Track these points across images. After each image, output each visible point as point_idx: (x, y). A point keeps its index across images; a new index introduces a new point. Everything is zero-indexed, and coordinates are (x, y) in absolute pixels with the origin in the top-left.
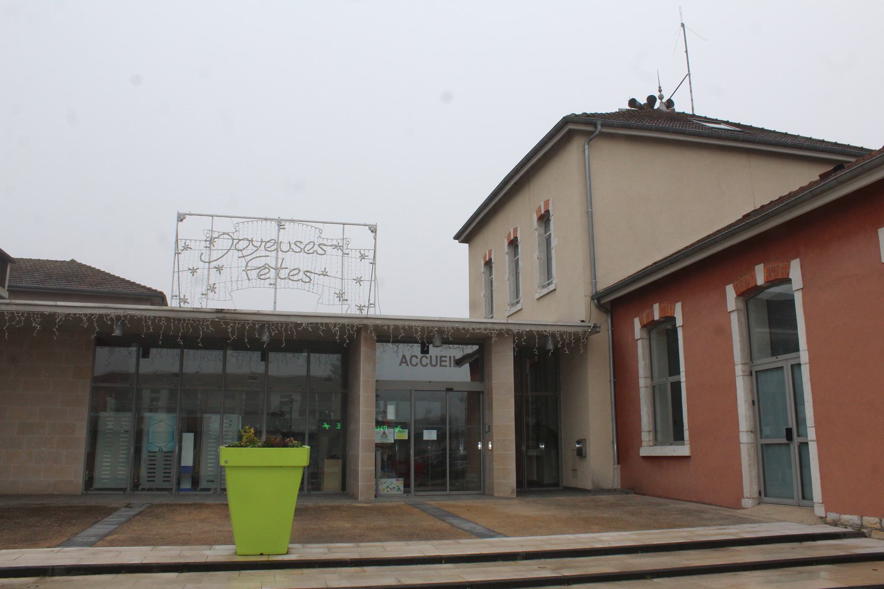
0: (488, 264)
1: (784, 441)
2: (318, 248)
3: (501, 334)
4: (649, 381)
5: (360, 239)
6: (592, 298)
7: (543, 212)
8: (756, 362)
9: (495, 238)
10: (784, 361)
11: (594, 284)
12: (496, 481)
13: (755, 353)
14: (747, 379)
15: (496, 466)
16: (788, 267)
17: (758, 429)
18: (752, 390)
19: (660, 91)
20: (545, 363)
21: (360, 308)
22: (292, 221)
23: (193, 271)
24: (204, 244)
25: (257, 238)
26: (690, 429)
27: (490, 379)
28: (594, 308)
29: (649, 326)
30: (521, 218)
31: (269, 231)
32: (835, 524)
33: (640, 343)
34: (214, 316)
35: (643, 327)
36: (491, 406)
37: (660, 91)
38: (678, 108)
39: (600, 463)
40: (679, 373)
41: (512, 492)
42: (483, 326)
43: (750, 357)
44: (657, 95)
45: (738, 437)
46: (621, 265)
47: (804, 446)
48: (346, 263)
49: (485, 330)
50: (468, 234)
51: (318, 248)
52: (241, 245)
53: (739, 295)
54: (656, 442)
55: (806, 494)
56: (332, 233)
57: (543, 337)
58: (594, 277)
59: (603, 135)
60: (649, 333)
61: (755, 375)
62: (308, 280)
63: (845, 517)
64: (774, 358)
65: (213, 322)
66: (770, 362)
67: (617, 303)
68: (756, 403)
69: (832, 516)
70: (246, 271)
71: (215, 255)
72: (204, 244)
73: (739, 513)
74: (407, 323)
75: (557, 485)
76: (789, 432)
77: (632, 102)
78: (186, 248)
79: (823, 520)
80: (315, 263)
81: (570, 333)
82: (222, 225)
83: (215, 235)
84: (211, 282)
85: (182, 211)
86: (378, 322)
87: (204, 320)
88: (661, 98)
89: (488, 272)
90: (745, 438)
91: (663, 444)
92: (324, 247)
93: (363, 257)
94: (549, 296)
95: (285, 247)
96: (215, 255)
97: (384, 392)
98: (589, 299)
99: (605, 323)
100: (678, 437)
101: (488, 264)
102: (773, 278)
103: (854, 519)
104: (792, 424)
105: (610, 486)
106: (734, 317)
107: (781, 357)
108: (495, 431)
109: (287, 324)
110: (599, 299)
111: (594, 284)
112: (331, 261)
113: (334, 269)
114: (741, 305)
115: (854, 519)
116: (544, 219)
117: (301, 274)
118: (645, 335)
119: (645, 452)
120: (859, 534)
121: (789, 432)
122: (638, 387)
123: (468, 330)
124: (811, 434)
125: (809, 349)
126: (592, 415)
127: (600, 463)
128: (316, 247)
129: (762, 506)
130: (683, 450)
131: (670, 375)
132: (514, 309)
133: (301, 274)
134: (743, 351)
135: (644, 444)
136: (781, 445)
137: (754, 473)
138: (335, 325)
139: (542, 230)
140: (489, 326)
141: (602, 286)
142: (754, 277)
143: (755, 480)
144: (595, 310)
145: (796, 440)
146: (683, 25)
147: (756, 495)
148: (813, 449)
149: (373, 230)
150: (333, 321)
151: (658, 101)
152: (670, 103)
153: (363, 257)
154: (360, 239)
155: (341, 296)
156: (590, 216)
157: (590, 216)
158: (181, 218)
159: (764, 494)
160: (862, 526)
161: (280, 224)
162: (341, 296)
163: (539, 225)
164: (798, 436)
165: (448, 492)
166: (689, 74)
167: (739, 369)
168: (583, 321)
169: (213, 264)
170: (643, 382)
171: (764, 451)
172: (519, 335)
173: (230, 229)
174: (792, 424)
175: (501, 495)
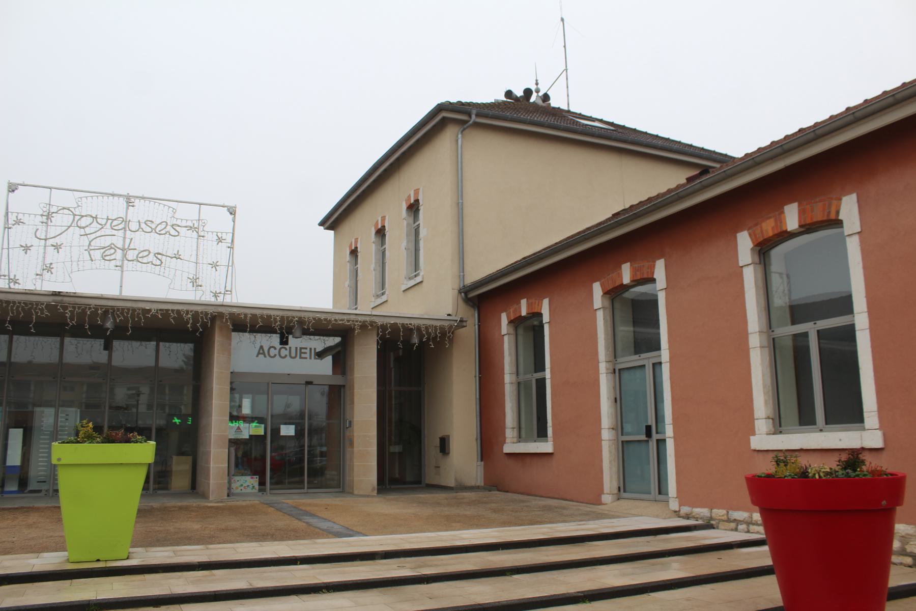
0: (354, 252)
1: (644, 437)
2: (171, 229)
3: (364, 326)
4: (514, 377)
5: (218, 221)
6: (460, 292)
8: (619, 360)
9: (361, 227)
10: (646, 359)
11: (462, 277)
14: (611, 376)
15: (357, 463)
16: (653, 267)
17: (620, 427)
18: (614, 388)
19: (537, 84)
20: (410, 357)
21: (216, 295)
22: (143, 198)
23: (26, 248)
24: (39, 219)
25: (102, 215)
28: (460, 300)
29: (517, 322)
31: (117, 208)
32: (687, 517)
33: (506, 338)
34: (50, 299)
36: (352, 402)
37: (537, 84)
38: (554, 103)
40: (544, 370)
41: (373, 490)
42: (345, 317)
43: (615, 354)
44: (533, 88)
45: (600, 433)
46: (491, 258)
47: (661, 443)
50: (335, 220)
52: (84, 222)
53: (606, 293)
54: (520, 439)
55: (662, 489)
56: (188, 213)
60: (516, 329)
61: (618, 373)
62: (158, 262)
63: (697, 510)
64: (637, 357)
65: (49, 306)
67: (484, 298)
68: (618, 401)
69: (685, 510)
70: (89, 250)
71: (52, 232)
72: (39, 219)
74: (265, 312)
76: (648, 429)
77: (509, 94)
78: (18, 222)
79: (677, 513)
80: (168, 245)
82: (61, 199)
83: (54, 209)
84: (48, 262)
85: (14, 181)
86: (234, 310)
87: (37, 303)
88: (538, 91)
90: (606, 435)
91: (527, 440)
92: (177, 228)
93: (220, 240)
94: (416, 287)
95: (134, 226)
96: (52, 232)
97: (778, 426)
98: (457, 292)
100: (542, 433)
101: (354, 252)
103: (704, 512)
104: (651, 421)
105: (473, 484)
106: (600, 315)
107: (643, 356)
109: (134, 310)
110: (466, 293)
111: (462, 277)
112: (186, 243)
114: (607, 303)
115: (704, 512)
116: (414, 208)
117: (151, 258)
118: (512, 331)
119: (508, 448)
120: (708, 526)
121: (648, 429)
122: (503, 384)
124: (669, 431)
127: (463, 460)
128: (169, 228)
129: (621, 502)
130: (546, 447)
133: (151, 258)
134: (607, 348)
136: (641, 441)
137: (615, 469)
138: (187, 312)
139: (411, 220)
142: (620, 276)
143: (615, 476)
144: (462, 304)
145: (655, 437)
146: (562, 20)
147: (616, 491)
148: (670, 446)
149: (232, 212)
150: (185, 308)
152: (546, 97)
153: (220, 240)
154: (218, 221)
160: (711, 518)
161: (129, 200)
163: (408, 215)
164: (657, 433)
167: (603, 367)
168: (449, 315)
169: (50, 242)
170: (508, 378)
171: (624, 447)
172: (384, 327)
173: (72, 204)
174: (651, 421)
175: (361, 493)
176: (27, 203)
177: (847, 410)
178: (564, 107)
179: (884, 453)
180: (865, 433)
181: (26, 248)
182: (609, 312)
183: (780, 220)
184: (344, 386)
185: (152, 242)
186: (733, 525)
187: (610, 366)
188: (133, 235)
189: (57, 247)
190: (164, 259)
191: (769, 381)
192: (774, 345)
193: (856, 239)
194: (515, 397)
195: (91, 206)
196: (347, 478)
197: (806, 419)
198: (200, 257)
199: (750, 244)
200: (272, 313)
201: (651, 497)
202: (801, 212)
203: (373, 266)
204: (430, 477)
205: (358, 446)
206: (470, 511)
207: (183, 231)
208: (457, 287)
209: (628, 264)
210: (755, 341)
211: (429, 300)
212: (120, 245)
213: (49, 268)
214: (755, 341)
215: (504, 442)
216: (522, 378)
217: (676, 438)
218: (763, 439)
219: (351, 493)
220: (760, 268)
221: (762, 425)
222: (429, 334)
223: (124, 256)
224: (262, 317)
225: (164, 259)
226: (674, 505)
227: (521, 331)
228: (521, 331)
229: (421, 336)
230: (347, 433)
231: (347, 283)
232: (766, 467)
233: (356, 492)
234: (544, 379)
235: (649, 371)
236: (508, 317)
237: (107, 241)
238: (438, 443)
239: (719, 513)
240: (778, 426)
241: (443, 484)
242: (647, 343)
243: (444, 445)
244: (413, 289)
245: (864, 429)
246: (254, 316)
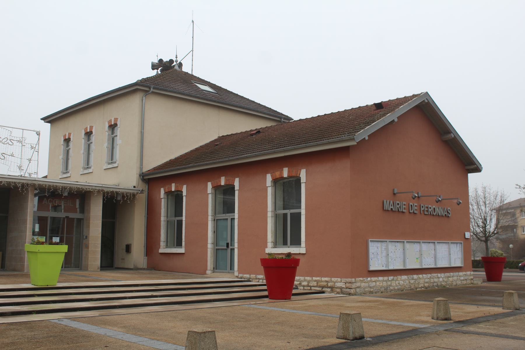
0: (67, 141)
1: (225, 248)
3: (99, 191)
4: (166, 218)
6: (140, 176)
7: (113, 123)
8: (217, 215)
10: (229, 216)
11: (141, 169)
12: (89, 263)
13: (217, 212)
14: (213, 222)
15: (90, 256)
17: (216, 242)
18: (214, 227)
19: (176, 57)
20: (115, 205)
21: (30, 174)
26: (185, 241)
27: (89, 212)
28: (140, 180)
29: (169, 193)
32: (241, 278)
33: (163, 200)
35: (166, 193)
36: (88, 227)
37: (176, 57)
38: (185, 69)
39: (138, 255)
40: (182, 216)
41: (98, 269)
42: (91, 187)
43: (215, 213)
44: (174, 59)
45: (207, 245)
46: (155, 159)
47: (232, 250)
48: (23, 150)
50: (52, 119)
54: (167, 246)
55: (232, 267)
56: (17, 134)
57: (117, 193)
59: (153, 93)
60: (168, 196)
61: (216, 221)
62: (3, 158)
63: (245, 275)
64: (224, 215)
66: (223, 216)
67: (152, 179)
68: (216, 232)
69: (241, 275)
73: (205, 275)
74: (55, 184)
76: (228, 244)
79: (237, 277)
80: (8, 149)
86: (41, 183)
88: (176, 61)
89: (66, 145)
90: (210, 246)
92: (12, 141)
93: (32, 148)
94: (113, 169)
97: (275, 245)
98: (138, 175)
100: (179, 244)
101: (67, 141)
102: (228, 183)
103: (247, 276)
105: (142, 267)
106: (210, 196)
110: (143, 177)
112: (16, 148)
113: (17, 153)
114: (213, 191)
115: (247, 276)
116: (113, 127)
119: (161, 251)
120: (249, 281)
121: (228, 244)
122: (160, 221)
124: (236, 245)
125: (238, 213)
126: (136, 233)
127: (138, 255)
128: (8, 141)
129: (214, 273)
130: (182, 250)
131: (176, 216)
134: (212, 210)
137: (212, 260)
139: (110, 132)
140: (94, 187)
141: (146, 169)
142: (220, 181)
143: (212, 263)
144: (141, 182)
145: (230, 247)
146: (193, 22)
147: (212, 269)
149: (38, 134)
150: (18, 181)
151: (175, 63)
155: (20, 168)
156: (142, 134)
157: (142, 134)
159: (216, 268)
160: (250, 278)
162: (20, 168)
163: (109, 130)
166: (193, 51)
167: (210, 218)
168: (134, 187)
170: (163, 219)
171: (217, 251)
175: (92, 270)
177: (296, 242)
178: (190, 72)
179: (306, 255)
180: (301, 249)
183: (282, 173)
184: (83, 219)
186: (258, 280)
187: (213, 217)
190: (6, 156)
191: (273, 230)
192: (276, 216)
193: (304, 184)
197: (285, 243)
198: (23, 155)
200: (58, 184)
201: (227, 271)
202: (289, 172)
205: (91, 248)
208: (138, 173)
209: (224, 177)
210: (270, 214)
214: (270, 214)
215: (159, 248)
216: (169, 219)
217: (239, 248)
218: (270, 250)
219: (86, 269)
221: (270, 245)
222: (127, 196)
224: (53, 186)
225: (6, 156)
226: (236, 274)
227: (170, 197)
228: (170, 197)
230: (84, 241)
232: (267, 257)
233: (89, 270)
235: (229, 221)
236: (165, 190)
238: (124, 247)
239: (253, 276)
240: (275, 245)
242: (229, 208)
243: (128, 249)
244: (111, 170)
245: (301, 247)
246: (49, 185)
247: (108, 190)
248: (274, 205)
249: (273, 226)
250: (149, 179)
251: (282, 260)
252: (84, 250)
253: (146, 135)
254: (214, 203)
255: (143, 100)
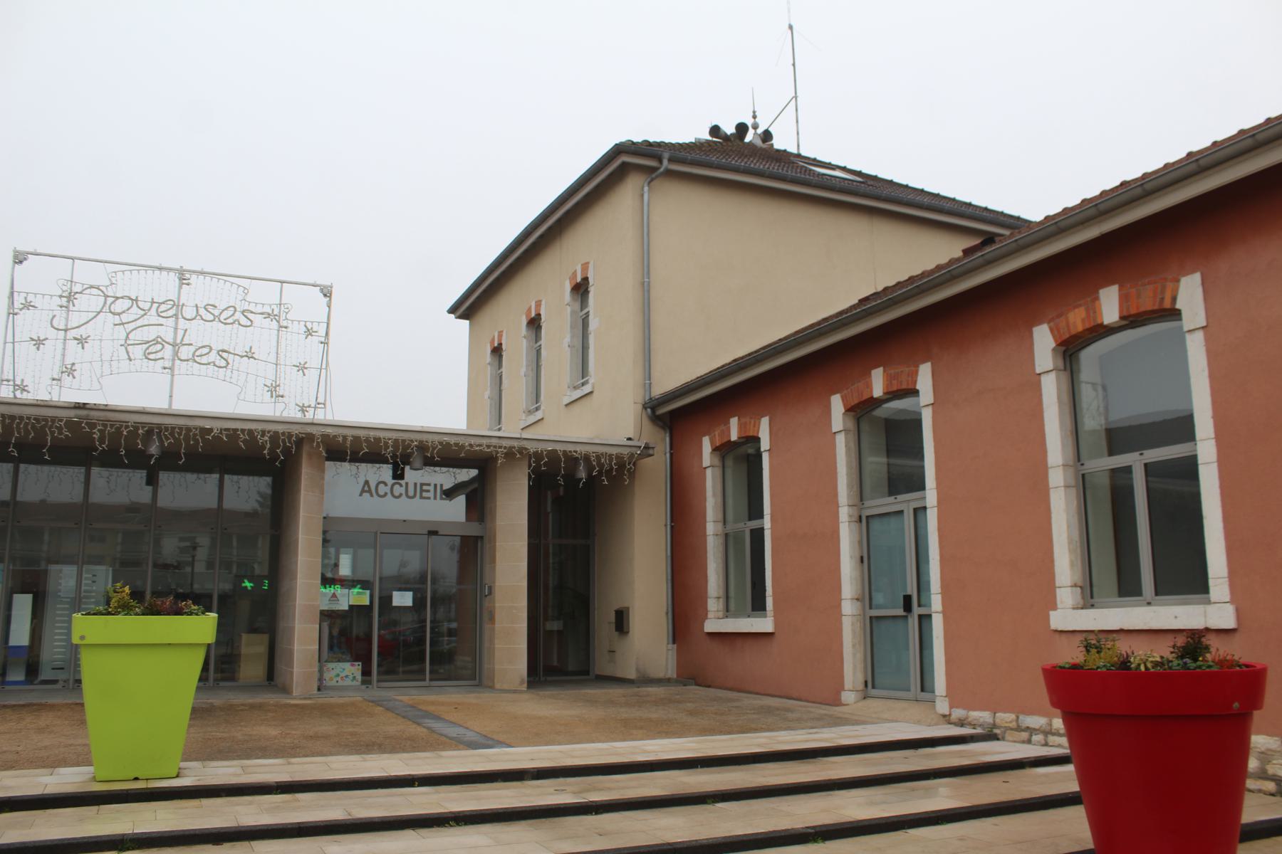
0: (497, 351)
1: (901, 612)
2: (241, 316)
3: (510, 454)
4: (720, 525)
6: (645, 407)
7: (579, 280)
8: (867, 503)
9: (508, 314)
10: (905, 502)
11: (648, 386)
12: (497, 667)
14: (855, 526)
15: (499, 645)
17: (867, 597)
18: (860, 542)
19: (754, 117)
20: (575, 497)
21: (303, 409)
22: (202, 273)
23: (39, 343)
24: (57, 301)
25: (145, 297)
29: (724, 450)
30: (546, 286)
31: (166, 287)
32: (961, 723)
33: (709, 472)
34: (72, 413)
36: (493, 560)
37: (754, 117)
38: (778, 143)
39: (648, 642)
41: (522, 683)
42: (485, 441)
43: (861, 495)
44: (749, 122)
45: (839, 606)
47: (925, 619)
49: (488, 447)
51: (241, 316)
52: (120, 306)
54: (728, 612)
55: (925, 684)
56: (264, 295)
57: (572, 460)
58: (648, 373)
59: (670, 174)
60: (723, 459)
61: (865, 521)
62: (223, 363)
63: (975, 715)
64: (891, 499)
65: (69, 423)
67: (679, 416)
68: (865, 560)
69: (958, 713)
72: (57, 301)
74: (372, 433)
75: (587, 673)
76: (907, 601)
77: (715, 130)
78: (28, 306)
79: (946, 718)
80: (237, 339)
81: (611, 455)
82: (87, 274)
83: (77, 288)
84: (68, 361)
85: (21, 248)
86: (329, 430)
87: (54, 419)
88: (755, 127)
90: (849, 608)
91: (737, 615)
92: (250, 316)
93: (309, 333)
95: (189, 312)
97: (1089, 596)
98: (640, 407)
99: (661, 443)
100: (758, 605)
101: (497, 351)
103: (984, 716)
104: (912, 589)
105: (661, 675)
106: (841, 441)
108: (498, 594)
109: (189, 429)
110: (653, 409)
111: (648, 386)
112: (261, 336)
114: (851, 424)
115: (984, 716)
116: (581, 289)
117: (213, 356)
118: (717, 462)
119: (711, 626)
121: (907, 601)
122: (705, 535)
123: (463, 446)
124: (936, 603)
127: (648, 642)
128: (238, 315)
129: (869, 702)
130: (763, 624)
132: (532, 419)
133: (213, 356)
134: (850, 486)
135: (710, 615)
136: (896, 617)
137: (860, 656)
138: (263, 433)
139: (577, 305)
140: (494, 441)
141: (659, 389)
142: (869, 386)
143: (860, 666)
144: (646, 422)
145: (917, 610)
146: (791, 27)
147: (861, 687)
149: (327, 293)
150: (260, 427)
152: (767, 136)
153: (309, 333)
154: (307, 306)
155: (274, 390)
156: (645, 288)
157: (645, 288)
158: (19, 259)
160: (994, 726)
161: (183, 276)
162: (274, 390)
163: (574, 299)
165: (427, 683)
166: (796, 97)
167: (844, 513)
168: (629, 439)
169: (71, 334)
170: (712, 528)
171: (873, 624)
172: (538, 456)
173: (103, 281)
174: (912, 589)
175: (506, 687)
176: (41, 279)
177: (1185, 576)
180: (1210, 608)
181: (39, 343)
182: (853, 437)
183: (1093, 308)
184: (482, 537)
185: (215, 335)
186: (1025, 735)
188: (187, 325)
189: (82, 341)
190: (231, 358)
192: (1084, 484)
193: (1200, 336)
194: (720, 555)
195: (130, 284)
196: (486, 666)
197: (1128, 587)
198: (282, 356)
199: (1051, 343)
200: (381, 435)
201: (910, 695)
202: (1124, 299)
203: (523, 370)
204: (602, 666)
205: (501, 622)
206: (656, 714)
207: (258, 320)
208: (640, 400)
210: (1057, 478)
211: (602, 419)
212: (170, 339)
213: (70, 371)
214: (1057, 478)
215: (706, 617)
218: (1068, 615)
219: (491, 687)
220: (1065, 377)
221: (1066, 595)
222: (601, 465)
223: (176, 353)
224: (367, 440)
225: (231, 358)
226: (942, 706)
227: (729, 462)
228: (729, 462)
229: (590, 468)
230: (486, 604)
231: (487, 393)
232: (1071, 654)
233: (498, 686)
234: (762, 530)
237: (151, 334)
238: (613, 618)
239: (1005, 718)
241: (619, 675)
242: (906, 480)
243: (621, 621)
245: (1209, 602)
247: (540, 447)
248: (1070, 442)
249: (1075, 521)
250: (672, 412)
251: (1158, 678)
252: (487, 627)
253: (654, 293)
254: (855, 464)
255: (642, 195)
